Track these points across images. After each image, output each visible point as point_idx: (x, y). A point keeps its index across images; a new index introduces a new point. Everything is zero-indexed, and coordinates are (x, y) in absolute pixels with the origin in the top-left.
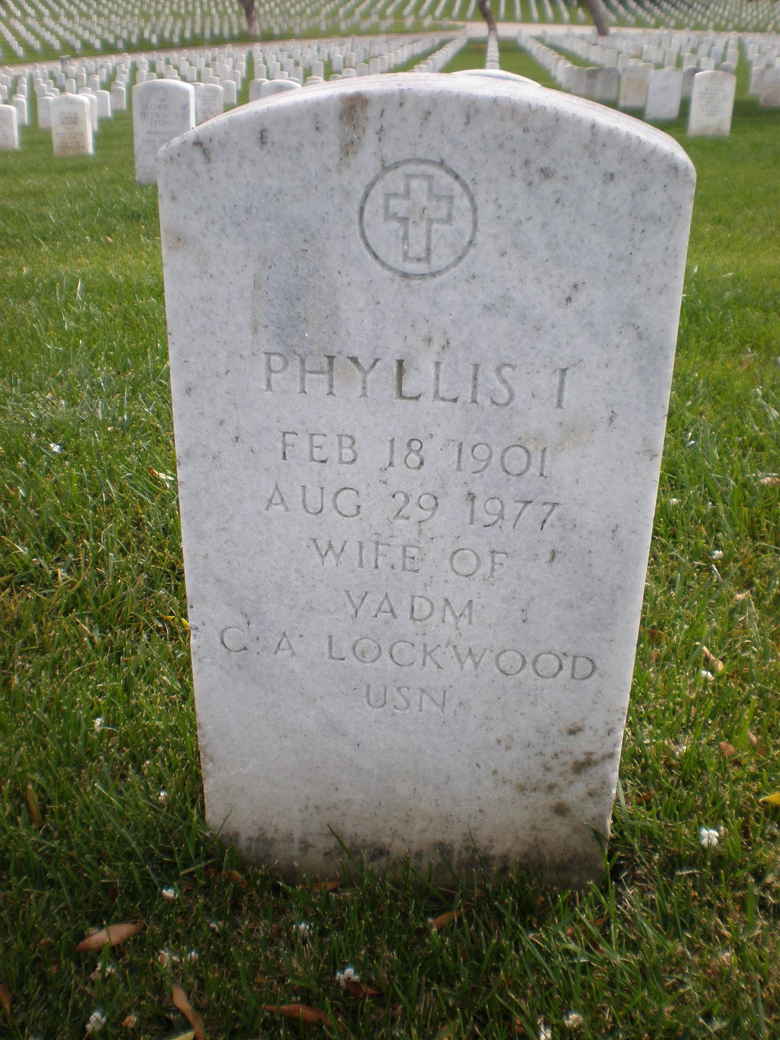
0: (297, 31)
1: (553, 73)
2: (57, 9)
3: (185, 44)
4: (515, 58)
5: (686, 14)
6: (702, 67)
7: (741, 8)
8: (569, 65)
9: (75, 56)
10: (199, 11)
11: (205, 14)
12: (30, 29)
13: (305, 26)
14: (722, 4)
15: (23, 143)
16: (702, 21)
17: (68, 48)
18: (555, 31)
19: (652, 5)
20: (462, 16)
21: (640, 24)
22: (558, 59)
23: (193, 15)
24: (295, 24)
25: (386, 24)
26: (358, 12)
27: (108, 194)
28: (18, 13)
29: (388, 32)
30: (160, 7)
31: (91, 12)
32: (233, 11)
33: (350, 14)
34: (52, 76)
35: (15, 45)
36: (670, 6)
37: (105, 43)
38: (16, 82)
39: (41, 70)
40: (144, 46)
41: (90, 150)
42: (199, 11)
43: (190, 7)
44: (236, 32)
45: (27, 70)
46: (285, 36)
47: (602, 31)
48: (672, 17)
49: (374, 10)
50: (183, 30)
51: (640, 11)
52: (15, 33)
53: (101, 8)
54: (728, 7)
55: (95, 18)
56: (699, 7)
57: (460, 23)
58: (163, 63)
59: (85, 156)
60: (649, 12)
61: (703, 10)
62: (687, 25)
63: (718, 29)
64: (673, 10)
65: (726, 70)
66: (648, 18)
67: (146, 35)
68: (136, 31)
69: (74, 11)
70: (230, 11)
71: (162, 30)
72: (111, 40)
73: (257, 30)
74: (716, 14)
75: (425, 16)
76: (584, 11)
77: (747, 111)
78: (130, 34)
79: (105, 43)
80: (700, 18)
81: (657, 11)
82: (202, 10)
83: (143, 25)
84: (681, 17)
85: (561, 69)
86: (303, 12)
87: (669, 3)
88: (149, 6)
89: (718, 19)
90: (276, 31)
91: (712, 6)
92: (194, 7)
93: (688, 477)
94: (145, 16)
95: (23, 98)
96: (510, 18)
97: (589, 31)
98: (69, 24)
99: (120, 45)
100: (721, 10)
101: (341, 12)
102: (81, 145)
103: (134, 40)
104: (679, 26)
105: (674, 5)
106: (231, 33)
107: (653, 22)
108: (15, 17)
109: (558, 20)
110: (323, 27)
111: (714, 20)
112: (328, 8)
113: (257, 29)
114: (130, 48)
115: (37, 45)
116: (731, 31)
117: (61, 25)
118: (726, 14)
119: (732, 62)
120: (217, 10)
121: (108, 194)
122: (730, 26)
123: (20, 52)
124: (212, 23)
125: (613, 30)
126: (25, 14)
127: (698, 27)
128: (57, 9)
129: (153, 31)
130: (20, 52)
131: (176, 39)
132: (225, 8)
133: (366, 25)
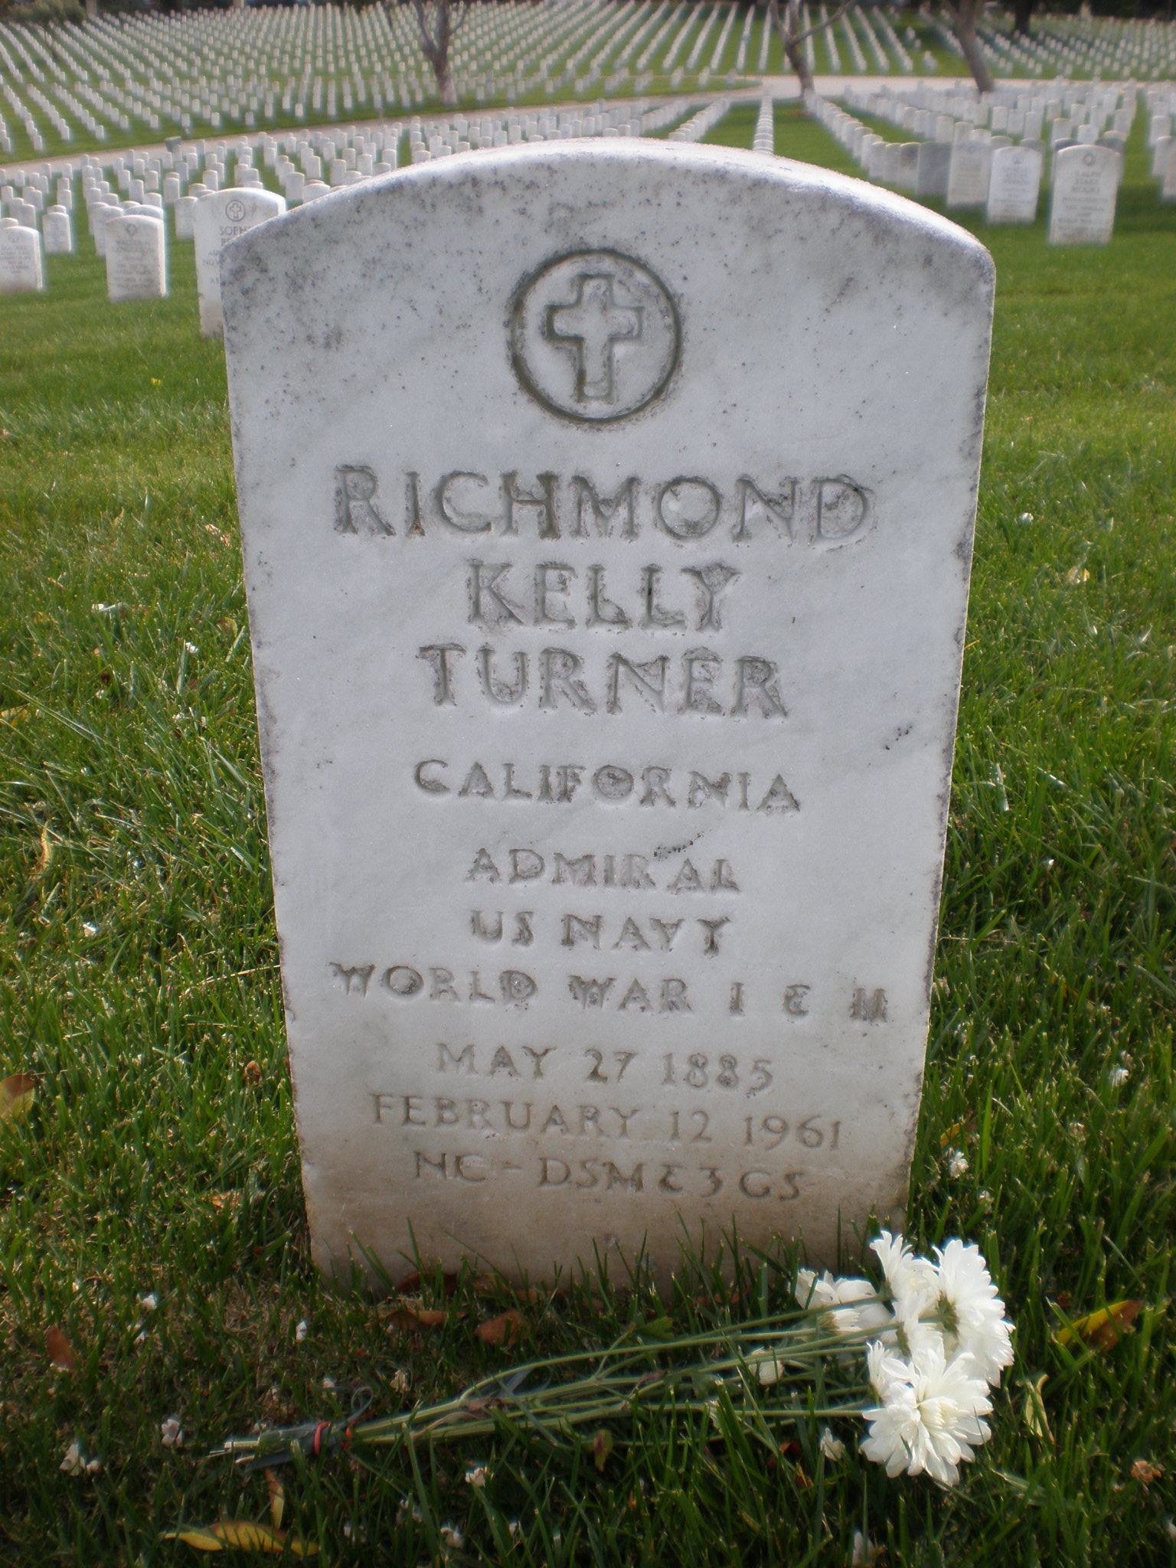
0: (511, 95)
1: (856, 154)
2: (142, 68)
3: (345, 118)
4: (800, 132)
5: (1086, 56)
6: (1079, 139)
7: (1166, 44)
8: (879, 141)
9: (186, 138)
10: (309, 68)
11: (368, 74)
12: (108, 98)
13: (522, 87)
14: (1138, 40)
15: (51, 282)
16: (1083, 65)
17: (170, 126)
18: (862, 88)
19: (1034, 45)
20: (751, 67)
21: (1019, 73)
22: (865, 132)
23: (297, 74)
24: (478, 85)
25: (644, 82)
26: (595, 64)
27: (140, 366)
28: (63, 76)
29: (647, 93)
30: (297, 64)
31: (195, 73)
32: (384, 68)
33: (584, 68)
34: (111, 175)
35: (91, 123)
36: (1059, 46)
37: (226, 119)
38: (55, 182)
39: (94, 164)
40: (284, 122)
41: (164, 289)
42: (309, 68)
43: (343, 63)
44: (419, 98)
45: (69, 166)
46: (496, 104)
47: (984, 86)
48: (1066, 62)
49: (618, 63)
50: (340, 98)
51: (1016, 54)
52: (87, 105)
53: (208, 67)
54: (1147, 44)
55: (203, 81)
56: (1104, 45)
57: (751, 79)
58: (275, 150)
59: (161, 300)
60: (1031, 54)
61: (1111, 48)
62: (1061, 72)
63: (1108, 76)
64: (1066, 51)
65: (1111, 144)
66: (1031, 64)
67: (287, 104)
68: (270, 100)
69: (170, 72)
70: (378, 68)
71: (310, 97)
72: (235, 113)
73: (452, 94)
74: (1131, 56)
75: (674, 68)
76: (934, 55)
77: (1139, 206)
78: (262, 105)
79: (226, 119)
80: (1107, 62)
81: (1041, 53)
82: (314, 67)
83: (277, 89)
84: (1052, 60)
85: (867, 145)
86: (512, 68)
87: (1058, 40)
88: (281, 63)
89: (1134, 63)
90: (481, 96)
91: (1122, 44)
92: (303, 63)
93: (76, 1549)
94: (274, 75)
95: (63, 212)
96: (824, 69)
97: (969, 83)
98: (140, 90)
99: (250, 120)
100: (1137, 50)
101: (570, 64)
102: (152, 282)
103: (269, 112)
104: (1049, 74)
105: (1066, 44)
106: (413, 100)
107: (1039, 69)
108: (59, 82)
109: (895, 70)
110: (550, 89)
111: (1102, 63)
112: (551, 59)
113: (454, 91)
114: (264, 125)
115: (125, 123)
116: (1126, 79)
117: (155, 93)
118: (1146, 55)
119: (1121, 132)
120: (361, 68)
121: (140, 366)
122: (1155, 73)
123: (101, 133)
124: (382, 85)
125: (1001, 83)
126: (73, 78)
127: (1079, 75)
128: (142, 68)
129: (295, 100)
130: (101, 133)
131: (332, 110)
132: (395, 64)
133: (613, 83)
